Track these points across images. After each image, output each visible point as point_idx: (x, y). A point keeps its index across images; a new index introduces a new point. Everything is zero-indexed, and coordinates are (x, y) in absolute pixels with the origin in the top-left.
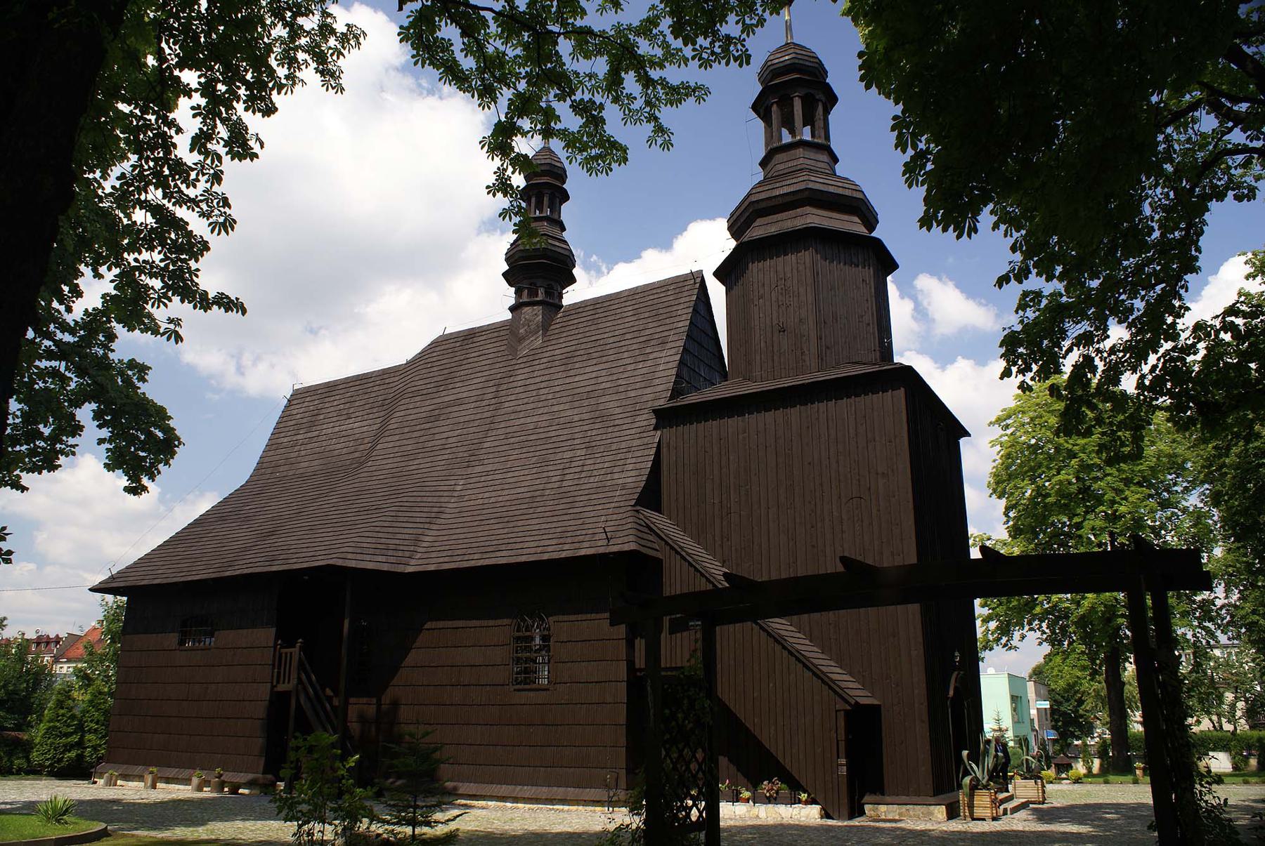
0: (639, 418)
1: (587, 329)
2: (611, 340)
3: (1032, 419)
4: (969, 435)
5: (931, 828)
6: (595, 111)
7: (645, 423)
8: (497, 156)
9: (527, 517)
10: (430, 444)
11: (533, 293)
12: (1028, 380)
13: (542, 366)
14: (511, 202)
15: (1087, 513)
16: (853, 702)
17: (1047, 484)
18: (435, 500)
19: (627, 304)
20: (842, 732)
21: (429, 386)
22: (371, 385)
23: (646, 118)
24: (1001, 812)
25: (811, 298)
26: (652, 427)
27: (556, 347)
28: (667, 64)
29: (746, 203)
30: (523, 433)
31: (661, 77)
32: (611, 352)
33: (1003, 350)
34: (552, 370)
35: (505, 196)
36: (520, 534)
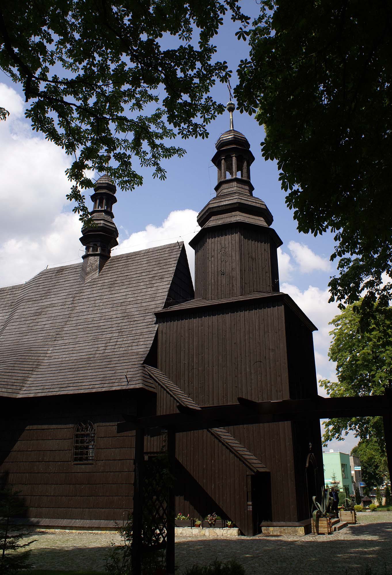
0: (147, 317)
1: (122, 269)
2: (135, 276)
3: (350, 321)
4: (317, 330)
5: (296, 540)
6: (126, 159)
7: (150, 320)
8: (74, 179)
9: (86, 368)
10: (36, 327)
11: (95, 250)
12: (343, 303)
13: (98, 288)
14: (79, 204)
15: (377, 369)
16: (255, 471)
17: (358, 354)
18: (36, 358)
19: (144, 257)
20: (250, 486)
21: (37, 296)
22: (6, 294)
23: (152, 163)
24: (333, 530)
25: (238, 258)
26: (154, 322)
27: (106, 278)
28: (164, 137)
29: (207, 208)
30: (86, 323)
31: (161, 143)
32: (134, 282)
33: (330, 288)
34: (103, 291)
35: (76, 200)
36: (81, 378)
